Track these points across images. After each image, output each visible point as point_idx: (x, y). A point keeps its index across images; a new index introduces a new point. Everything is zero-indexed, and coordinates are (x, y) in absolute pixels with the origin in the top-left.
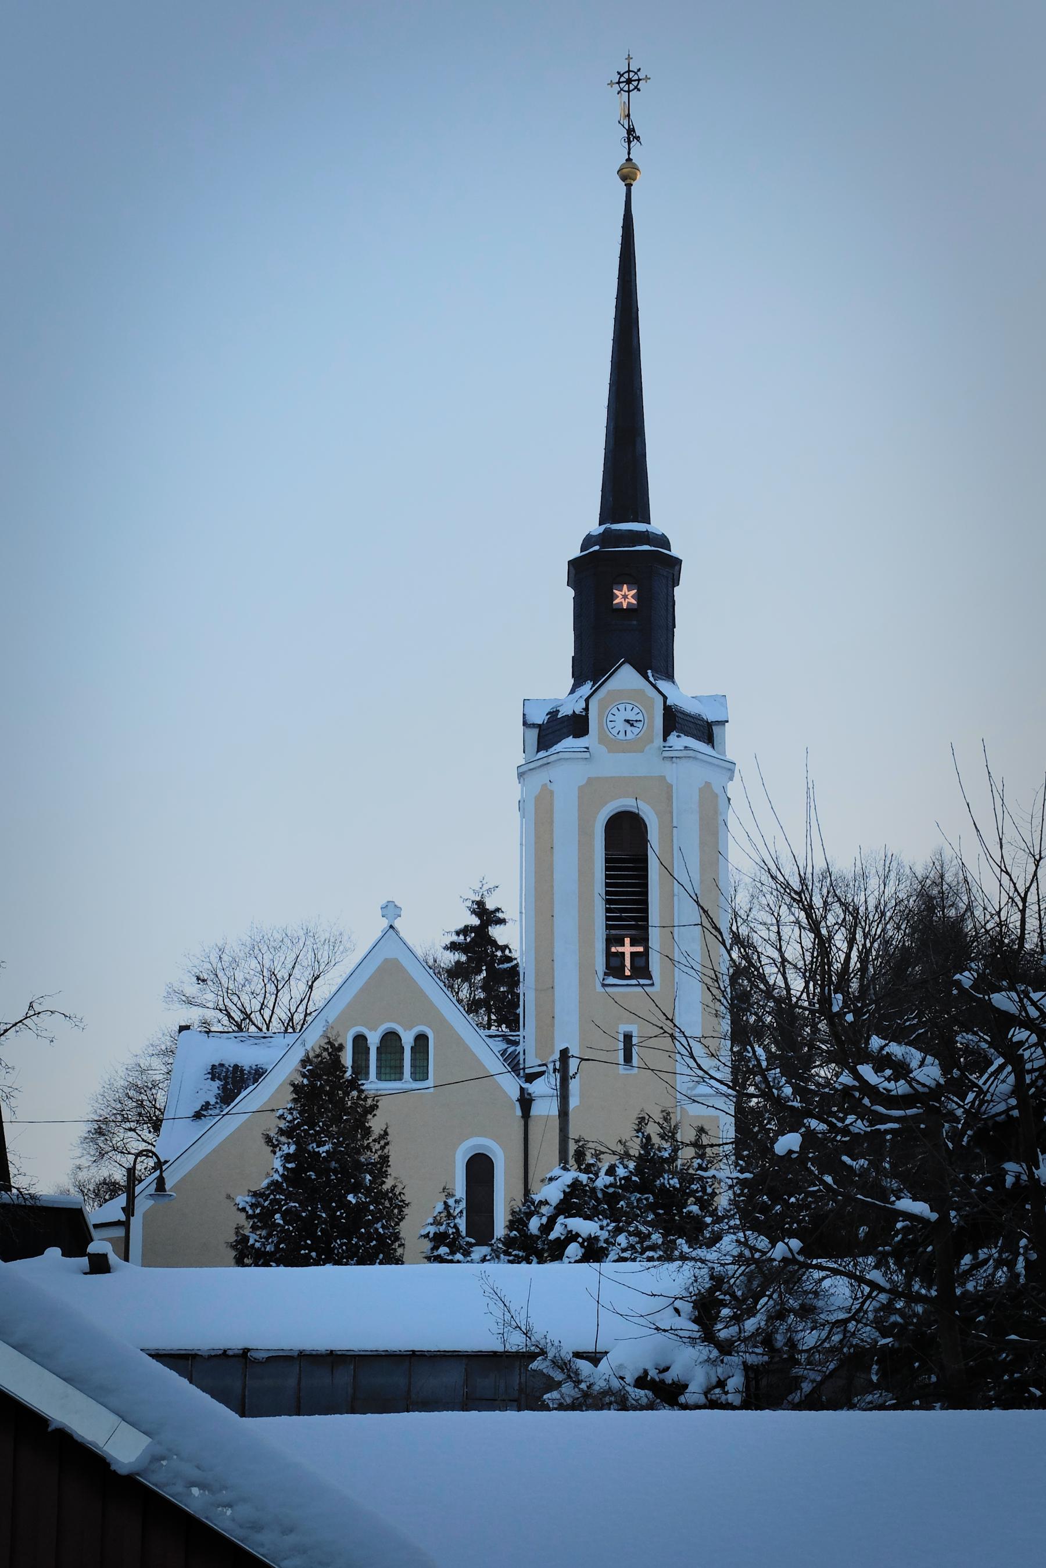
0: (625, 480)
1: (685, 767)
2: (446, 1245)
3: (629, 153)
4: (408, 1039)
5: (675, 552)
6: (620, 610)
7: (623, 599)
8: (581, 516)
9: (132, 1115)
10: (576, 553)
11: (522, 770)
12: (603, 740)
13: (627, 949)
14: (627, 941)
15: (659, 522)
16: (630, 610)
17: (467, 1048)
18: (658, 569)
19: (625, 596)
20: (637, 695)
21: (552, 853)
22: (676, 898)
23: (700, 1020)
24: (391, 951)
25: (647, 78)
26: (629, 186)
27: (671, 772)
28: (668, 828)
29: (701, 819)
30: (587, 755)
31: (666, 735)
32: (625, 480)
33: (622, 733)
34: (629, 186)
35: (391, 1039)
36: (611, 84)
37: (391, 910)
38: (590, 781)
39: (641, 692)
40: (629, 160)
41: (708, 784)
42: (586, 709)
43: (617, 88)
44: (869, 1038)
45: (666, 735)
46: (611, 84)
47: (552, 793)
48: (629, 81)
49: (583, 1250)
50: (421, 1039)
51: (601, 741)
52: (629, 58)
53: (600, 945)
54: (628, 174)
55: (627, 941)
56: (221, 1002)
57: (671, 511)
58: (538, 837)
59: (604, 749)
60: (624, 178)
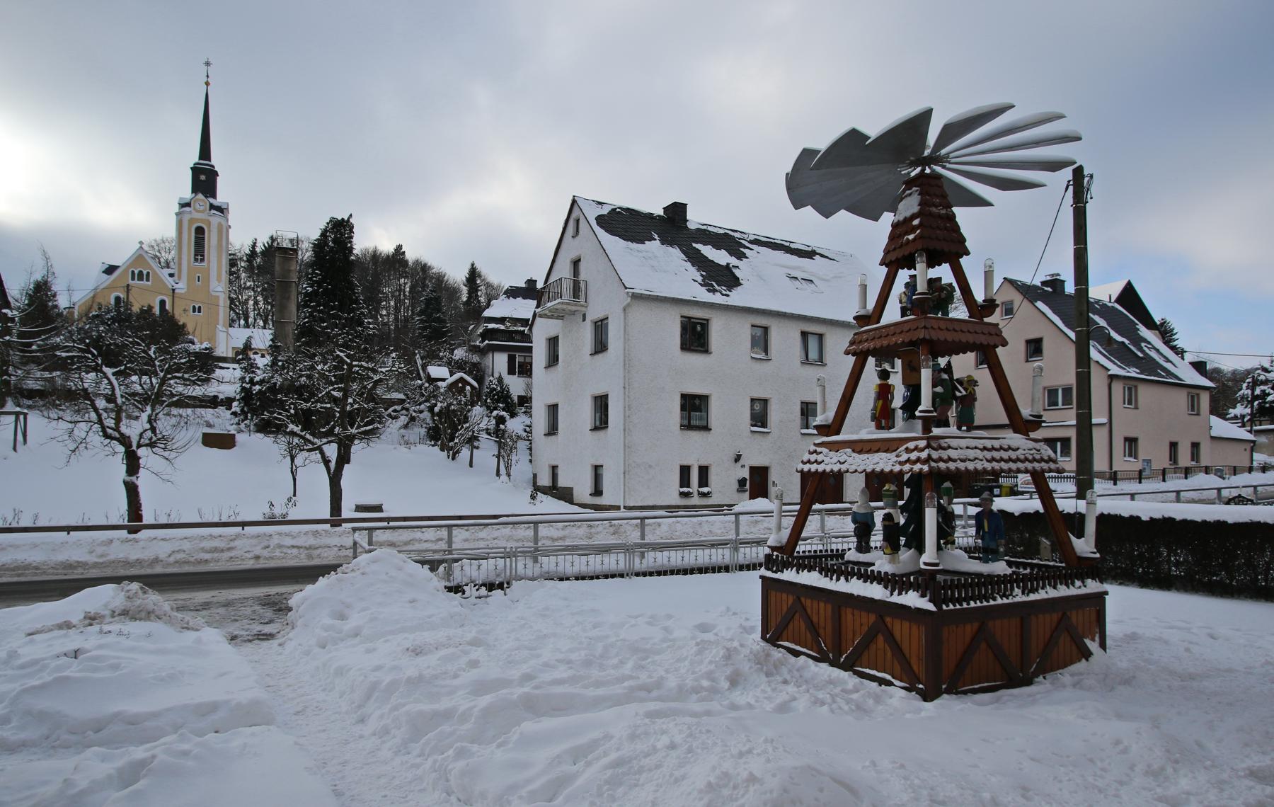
0: (205, 151)
1: (215, 219)
7: (204, 180)
15: (213, 162)
17: (1221, 525)
18: (212, 174)
19: (203, 177)
27: (211, 219)
32: (205, 151)
35: (141, 272)
44: (460, 346)
49: (692, 226)
57: (217, 160)
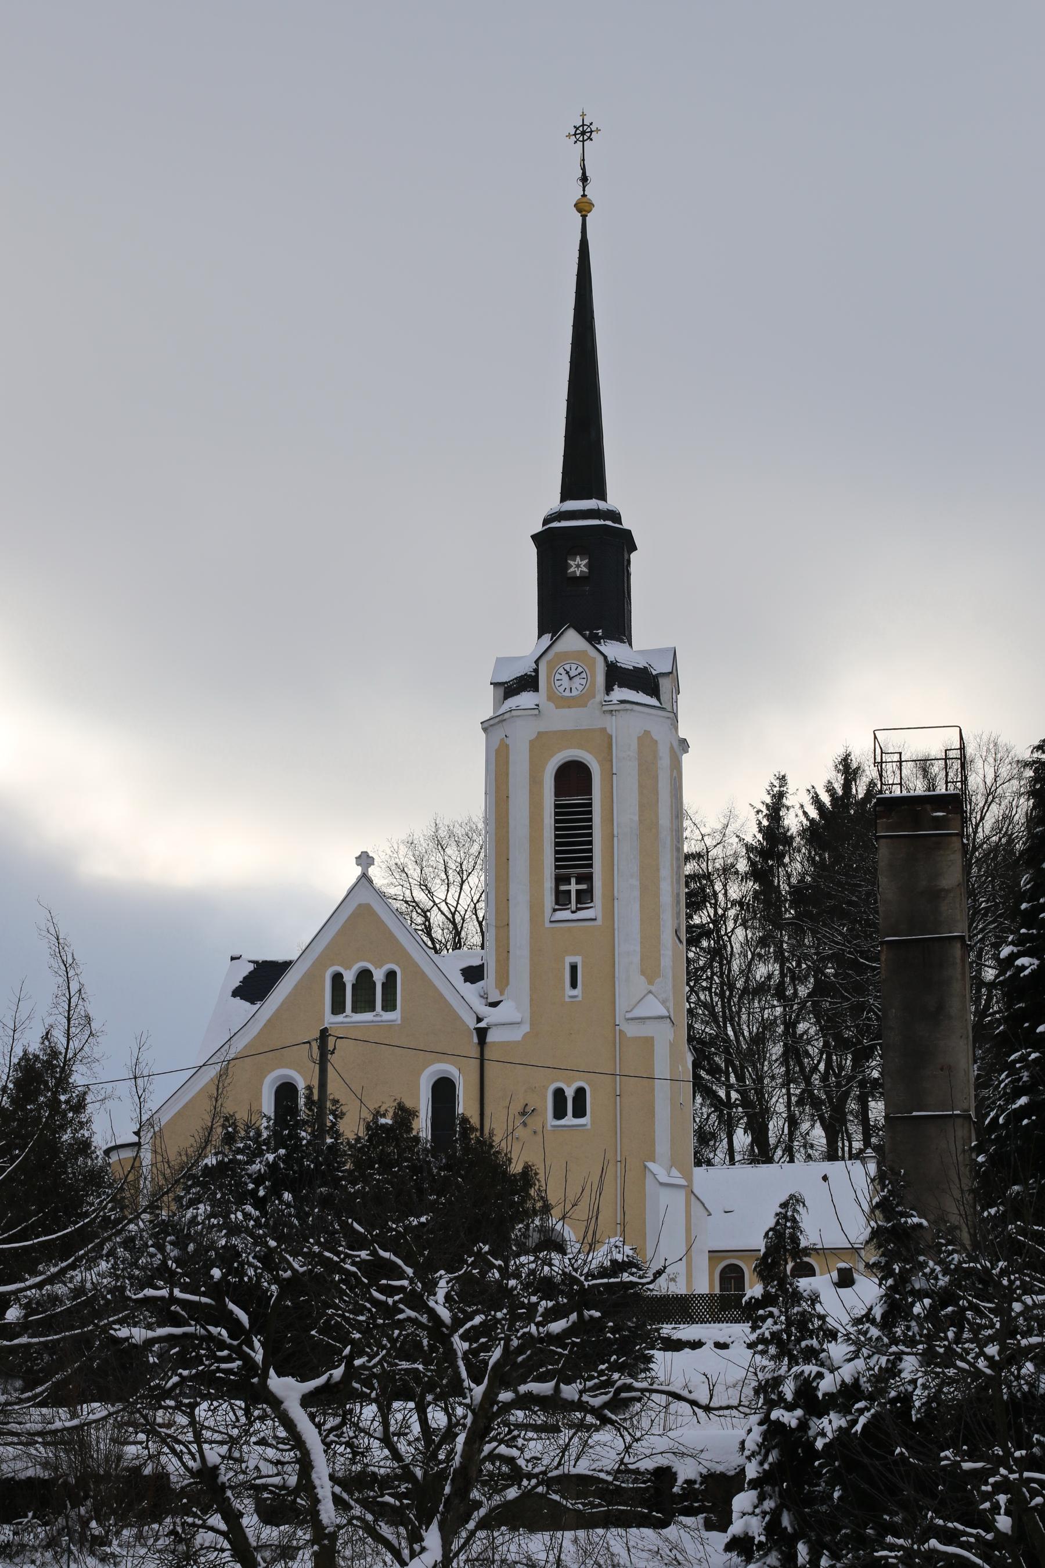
0: (584, 464)
1: (630, 719)
2: (140, 1138)
3: (584, 190)
4: (379, 976)
5: (626, 525)
6: (574, 579)
8: (543, 494)
9: (482, 1025)
10: (539, 528)
11: (486, 725)
12: (551, 697)
13: (573, 887)
14: (573, 881)
16: (582, 579)
20: (580, 655)
21: (507, 801)
22: (615, 839)
23: (638, 949)
24: (364, 897)
25: (598, 130)
26: (584, 217)
27: (611, 724)
28: (609, 775)
29: (640, 765)
30: (536, 712)
31: (609, 689)
32: (584, 464)
33: (568, 690)
34: (584, 217)
35: (365, 976)
36: (569, 136)
37: (365, 860)
38: (540, 734)
39: (585, 652)
40: (584, 196)
41: (647, 733)
42: (536, 671)
43: (573, 139)
45: (609, 689)
46: (569, 136)
47: (507, 746)
48: (583, 133)
50: (391, 975)
51: (550, 698)
52: (583, 115)
53: (549, 884)
54: (583, 207)
55: (573, 881)
56: (408, 893)
58: (497, 788)
59: (551, 705)
60: (579, 211)
